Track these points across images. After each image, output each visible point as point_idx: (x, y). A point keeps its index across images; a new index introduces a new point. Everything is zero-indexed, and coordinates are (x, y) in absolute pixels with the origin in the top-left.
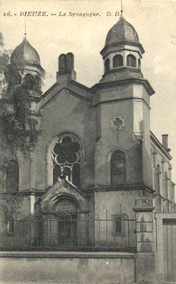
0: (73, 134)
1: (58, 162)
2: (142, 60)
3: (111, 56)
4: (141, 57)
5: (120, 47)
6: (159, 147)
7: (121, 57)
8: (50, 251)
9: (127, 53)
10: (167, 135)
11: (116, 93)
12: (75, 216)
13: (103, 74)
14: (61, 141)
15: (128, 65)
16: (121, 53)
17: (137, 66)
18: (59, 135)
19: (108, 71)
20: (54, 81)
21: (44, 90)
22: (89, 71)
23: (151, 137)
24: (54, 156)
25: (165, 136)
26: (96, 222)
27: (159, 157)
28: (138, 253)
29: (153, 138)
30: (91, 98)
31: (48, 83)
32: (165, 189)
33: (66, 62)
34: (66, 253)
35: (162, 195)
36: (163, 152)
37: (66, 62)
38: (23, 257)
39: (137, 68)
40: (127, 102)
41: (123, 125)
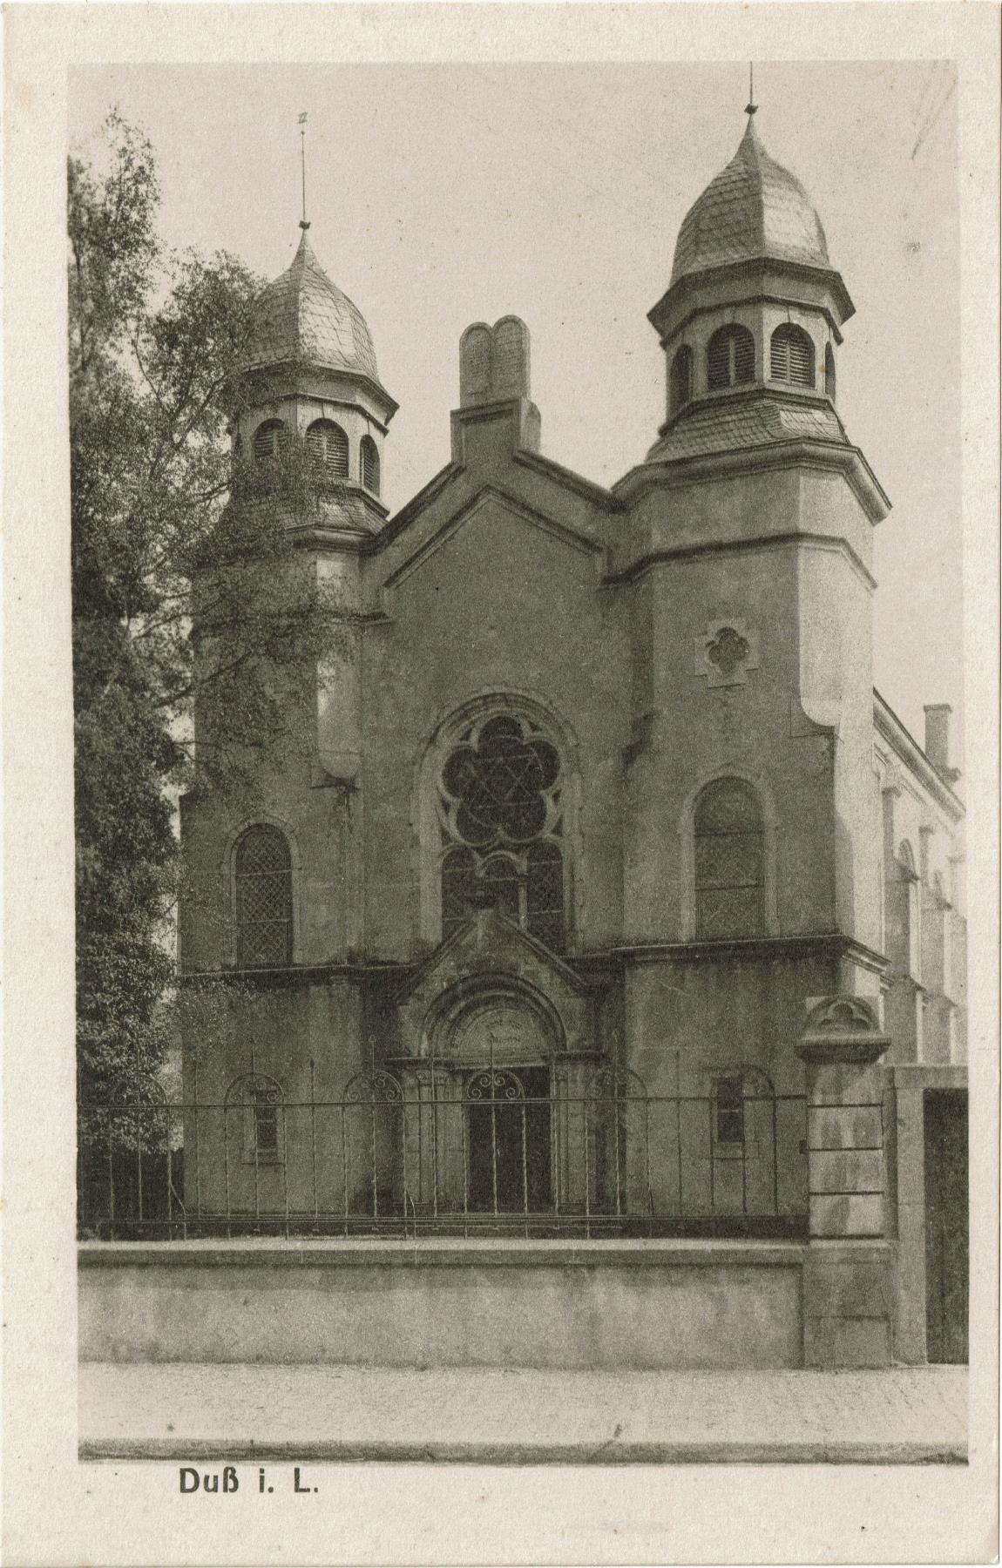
0: (528, 703)
1: (464, 835)
2: (838, 351)
3: (699, 337)
4: (839, 341)
5: (740, 314)
6: (909, 760)
7: (743, 336)
8: (555, 1235)
9: (773, 318)
10: (946, 707)
11: (724, 511)
12: (537, 1081)
13: (661, 418)
14: (475, 737)
15: (777, 374)
16: (744, 317)
17: (820, 378)
18: (464, 713)
19: (684, 409)
20: (442, 456)
21: (395, 495)
22: (602, 414)
23: (876, 714)
24: (446, 807)
25: (937, 715)
26: (631, 1107)
27: (909, 811)
28: (816, 1244)
29: (884, 721)
30: (619, 546)
31: (414, 453)
32: (774, 1258)
33: (494, 365)
34: (296, 1245)
35: (918, 980)
36: (929, 786)
37: (494, 365)
38: (370, 1266)
39: (819, 390)
40: (759, 560)
41: (753, 659)
